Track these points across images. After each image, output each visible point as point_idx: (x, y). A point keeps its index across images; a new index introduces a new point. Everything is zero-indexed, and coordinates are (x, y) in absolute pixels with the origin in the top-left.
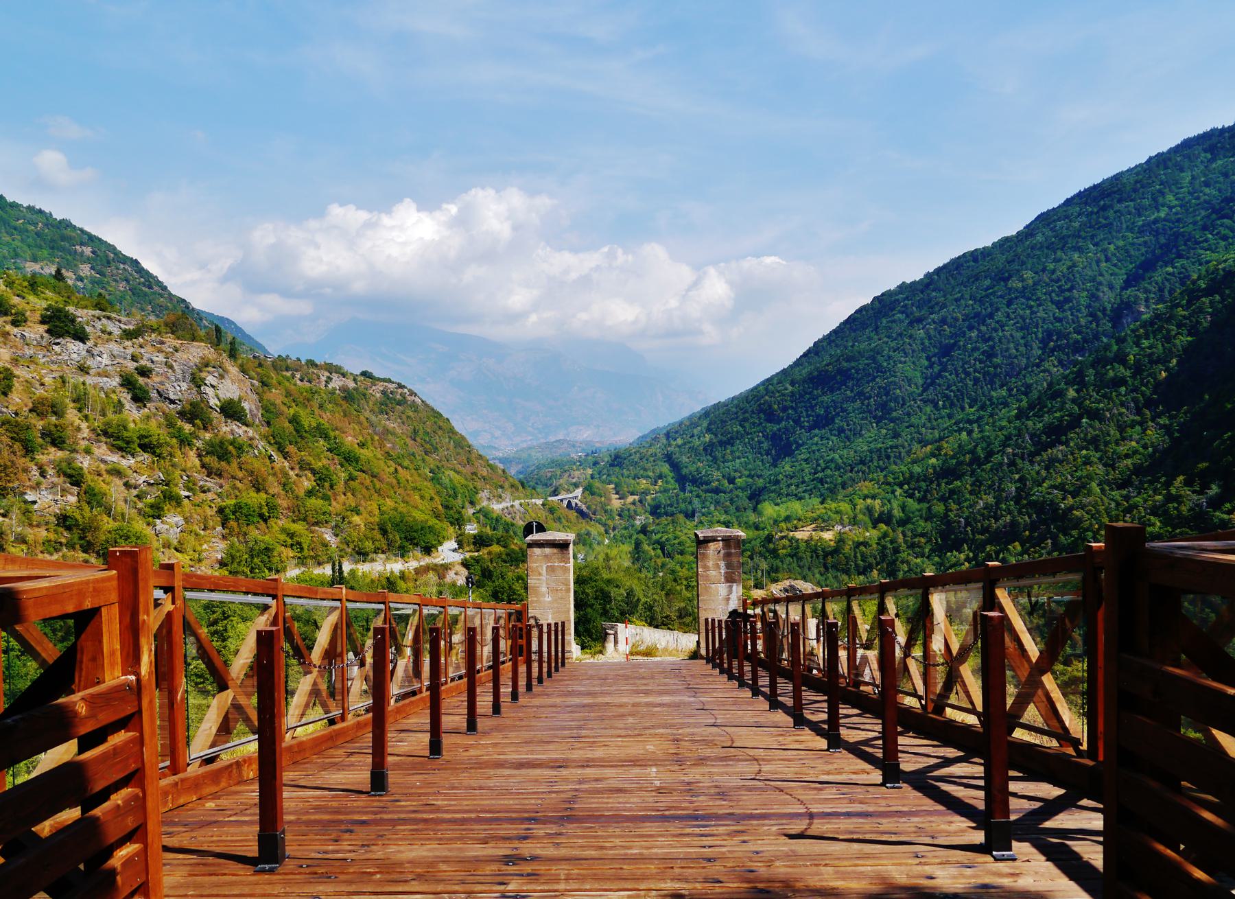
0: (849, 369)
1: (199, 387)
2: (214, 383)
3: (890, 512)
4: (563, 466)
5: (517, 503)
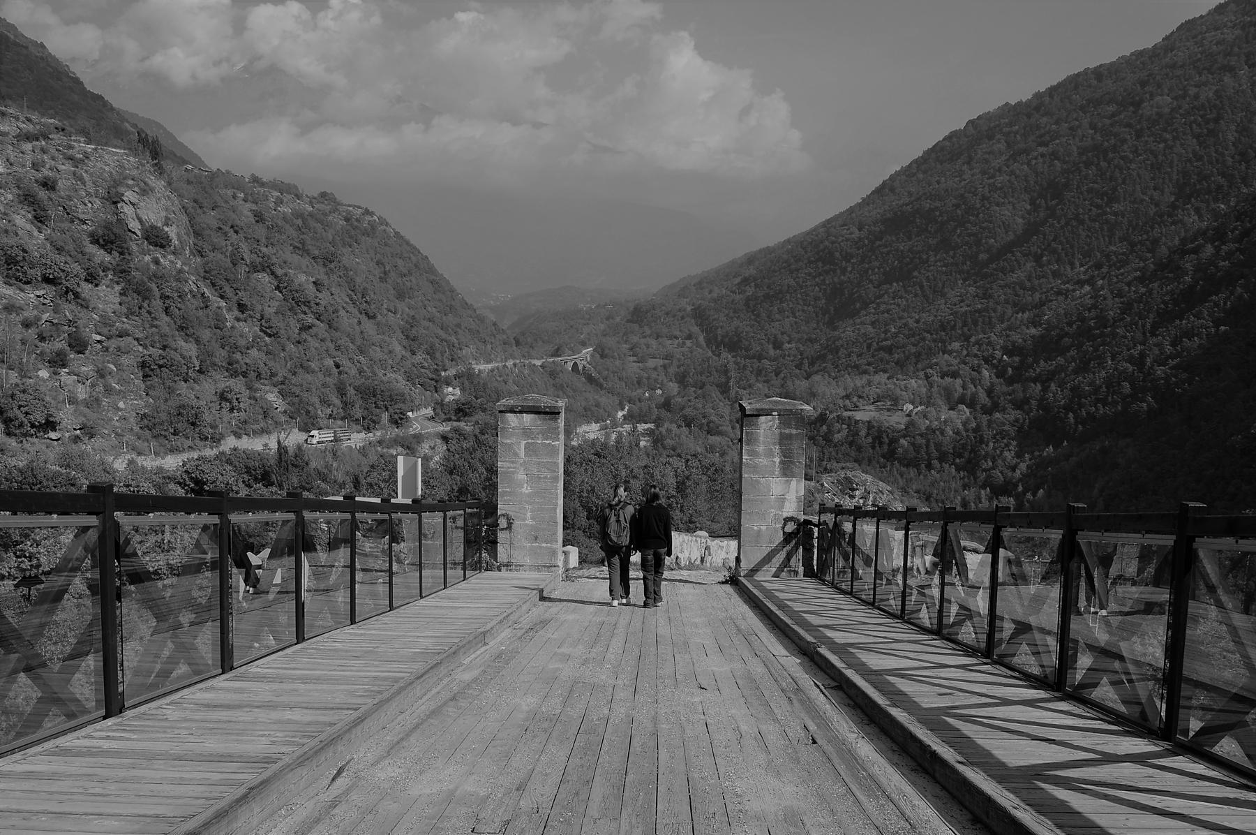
1: (115, 203)
3: (974, 396)
5: (510, 363)
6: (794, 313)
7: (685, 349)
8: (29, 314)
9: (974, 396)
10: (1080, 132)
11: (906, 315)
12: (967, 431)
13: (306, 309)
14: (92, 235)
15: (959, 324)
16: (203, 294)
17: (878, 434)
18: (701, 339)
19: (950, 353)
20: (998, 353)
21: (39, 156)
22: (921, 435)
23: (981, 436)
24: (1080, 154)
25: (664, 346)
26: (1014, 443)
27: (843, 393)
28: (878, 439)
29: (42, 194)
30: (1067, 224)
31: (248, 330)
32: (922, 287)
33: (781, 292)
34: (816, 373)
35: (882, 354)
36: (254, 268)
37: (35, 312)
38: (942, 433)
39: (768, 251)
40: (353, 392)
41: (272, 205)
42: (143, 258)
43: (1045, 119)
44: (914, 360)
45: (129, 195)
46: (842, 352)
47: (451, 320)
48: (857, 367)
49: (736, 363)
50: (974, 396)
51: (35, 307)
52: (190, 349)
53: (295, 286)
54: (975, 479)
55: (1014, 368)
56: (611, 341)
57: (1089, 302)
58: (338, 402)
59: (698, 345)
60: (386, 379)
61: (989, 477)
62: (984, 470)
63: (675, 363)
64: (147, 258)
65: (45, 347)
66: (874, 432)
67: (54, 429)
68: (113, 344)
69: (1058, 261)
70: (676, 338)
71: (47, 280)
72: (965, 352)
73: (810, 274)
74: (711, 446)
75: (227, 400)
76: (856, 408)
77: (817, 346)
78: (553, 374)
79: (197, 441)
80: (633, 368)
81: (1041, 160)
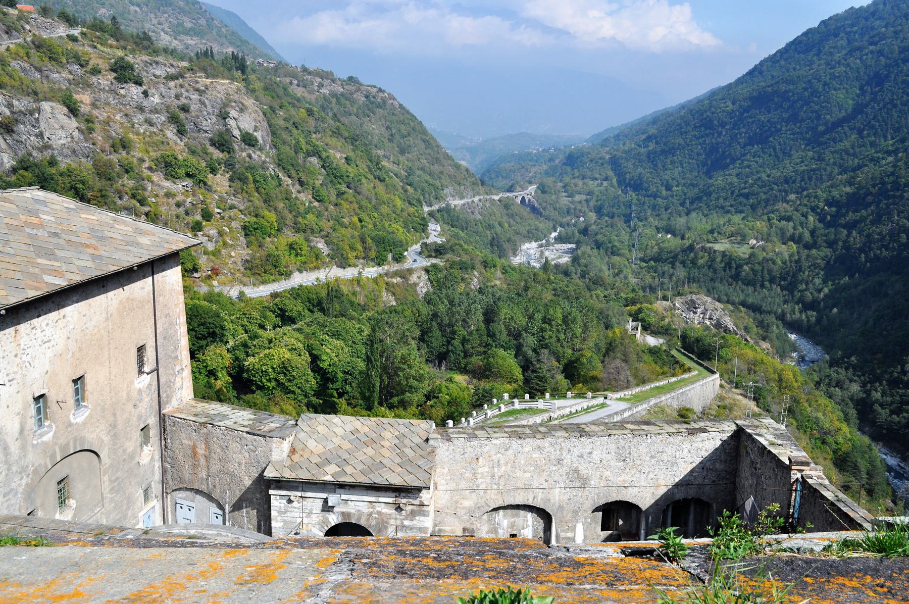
0: (786, 92)
1: (225, 118)
2: (236, 116)
3: (801, 235)
4: (524, 160)
5: (476, 199)
6: (681, 164)
7: (602, 188)
8: (180, 198)
9: (801, 235)
10: (901, 35)
11: (761, 169)
12: (791, 262)
13: (341, 181)
14: (211, 140)
15: (799, 179)
16: (278, 177)
17: (729, 261)
18: (614, 180)
19: (787, 202)
20: (821, 204)
21: (179, 90)
22: (759, 263)
23: (800, 266)
24: (900, 52)
25: (587, 186)
26: (822, 273)
27: (709, 228)
28: (728, 265)
29: (182, 115)
30: (884, 106)
31: (305, 197)
32: (775, 149)
33: (673, 148)
34: (694, 210)
35: (742, 199)
36: (309, 154)
37: (183, 197)
38: (774, 262)
39: (667, 114)
40: (370, 241)
41: (316, 88)
42: (242, 153)
43: (878, 22)
44: (764, 204)
45: (233, 113)
46: (714, 196)
47: (436, 168)
48: (723, 207)
49: (638, 200)
50: (801, 236)
51: (183, 194)
52: (271, 216)
53: (334, 165)
54: (793, 297)
55: (832, 216)
56: (549, 181)
57: (890, 169)
58: (361, 248)
59: (612, 186)
60: (390, 230)
61: (802, 296)
62: (800, 291)
63: (594, 198)
64: (244, 154)
65: (189, 219)
66: (726, 259)
67: (197, 271)
68: (226, 214)
69: (875, 134)
70: (597, 179)
71: (188, 175)
72: (798, 202)
73: (695, 136)
74: (613, 264)
75: (294, 249)
76: (716, 241)
77: (696, 190)
78: (506, 207)
79: (277, 276)
80: (564, 201)
81: (870, 56)
